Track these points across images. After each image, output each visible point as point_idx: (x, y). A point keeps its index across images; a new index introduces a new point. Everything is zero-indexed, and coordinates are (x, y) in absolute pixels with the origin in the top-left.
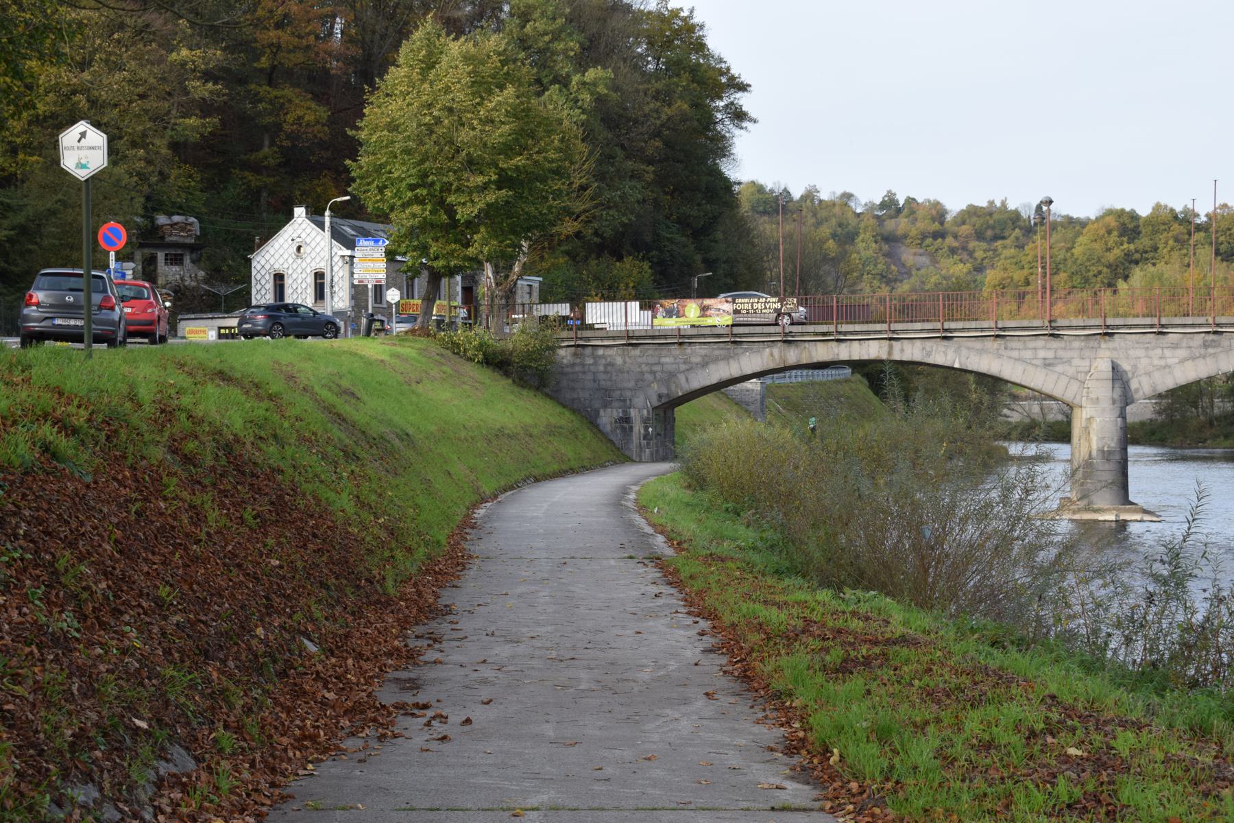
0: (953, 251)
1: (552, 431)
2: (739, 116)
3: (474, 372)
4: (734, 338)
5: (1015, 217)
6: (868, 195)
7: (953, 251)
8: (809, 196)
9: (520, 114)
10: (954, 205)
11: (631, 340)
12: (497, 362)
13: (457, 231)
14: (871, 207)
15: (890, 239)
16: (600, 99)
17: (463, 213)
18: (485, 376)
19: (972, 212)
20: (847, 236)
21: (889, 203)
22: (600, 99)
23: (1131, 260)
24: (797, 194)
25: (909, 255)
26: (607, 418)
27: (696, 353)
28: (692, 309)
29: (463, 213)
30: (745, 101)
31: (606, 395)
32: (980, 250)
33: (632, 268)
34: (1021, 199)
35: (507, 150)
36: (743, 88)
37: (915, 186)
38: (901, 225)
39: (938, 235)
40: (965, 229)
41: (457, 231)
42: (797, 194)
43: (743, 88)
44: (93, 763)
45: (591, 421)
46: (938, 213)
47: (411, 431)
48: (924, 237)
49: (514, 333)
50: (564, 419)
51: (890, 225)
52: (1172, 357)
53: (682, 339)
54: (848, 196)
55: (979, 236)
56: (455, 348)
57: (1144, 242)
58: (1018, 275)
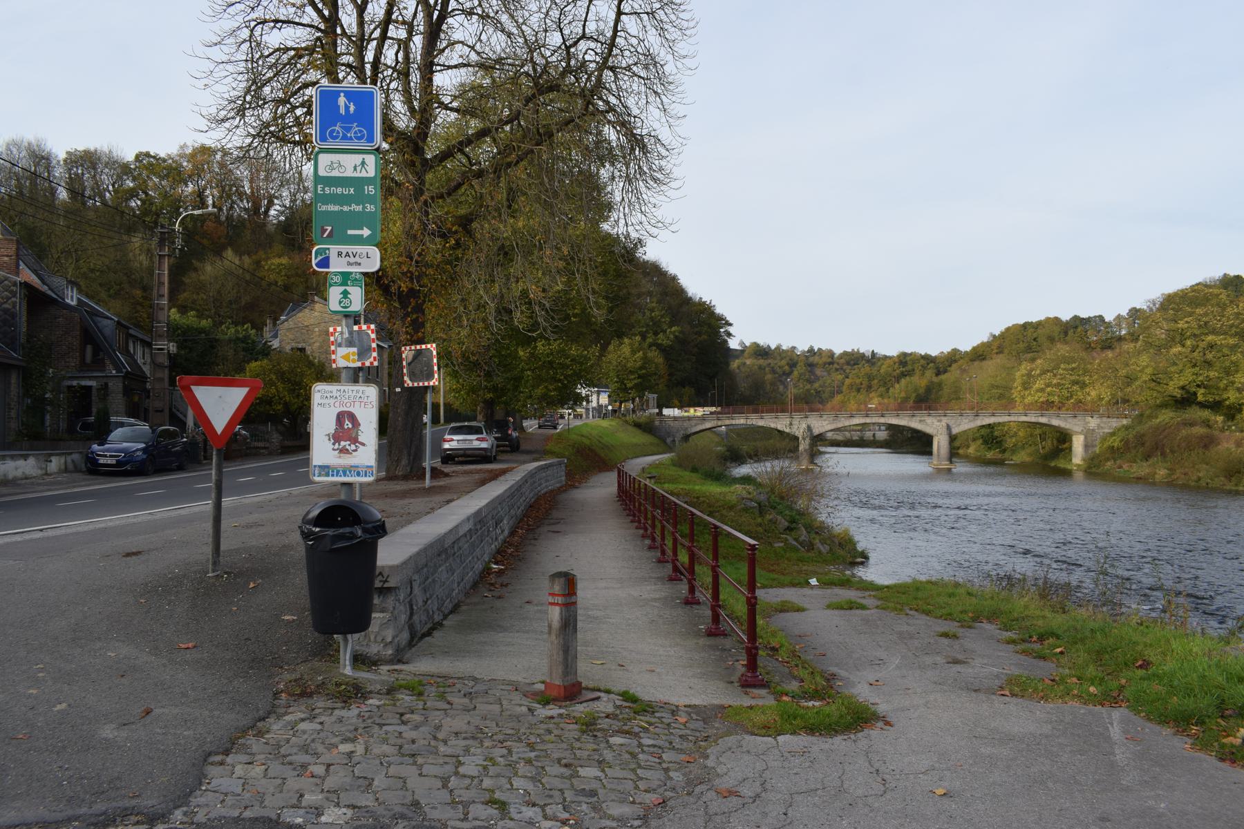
0: (837, 370)
1: (652, 444)
2: (729, 335)
3: (631, 429)
4: (703, 418)
5: (863, 355)
6: (802, 347)
7: (837, 370)
8: (778, 348)
9: (645, 358)
10: (838, 351)
11: (675, 419)
12: (638, 425)
13: (625, 390)
14: (803, 352)
15: (811, 365)
16: (676, 337)
17: (628, 386)
18: (634, 429)
19: (845, 354)
20: (793, 365)
21: (811, 350)
22: (676, 337)
23: (903, 375)
24: (773, 347)
25: (818, 372)
26: (669, 440)
27: (693, 422)
28: (692, 410)
29: (628, 386)
30: (731, 329)
31: (669, 434)
32: (847, 368)
33: (688, 391)
34: (865, 348)
35: (641, 368)
36: (731, 325)
37: (822, 342)
38: (816, 359)
39: (831, 363)
40: (842, 361)
41: (625, 390)
42: (773, 347)
43: (731, 325)
44: (304, 766)
45: (664, 442)
46: (831, 354)
47: (1059, 576)
48: (825, 364)
49: (643, 416)
50: (655, 440)
51: (811, 359)
52: (825, 423)
53: (689, 418)
54: (794, 348)
55: (848, 363)
56: (626, 422)
57: (910, 367)
58: (858, 381)
